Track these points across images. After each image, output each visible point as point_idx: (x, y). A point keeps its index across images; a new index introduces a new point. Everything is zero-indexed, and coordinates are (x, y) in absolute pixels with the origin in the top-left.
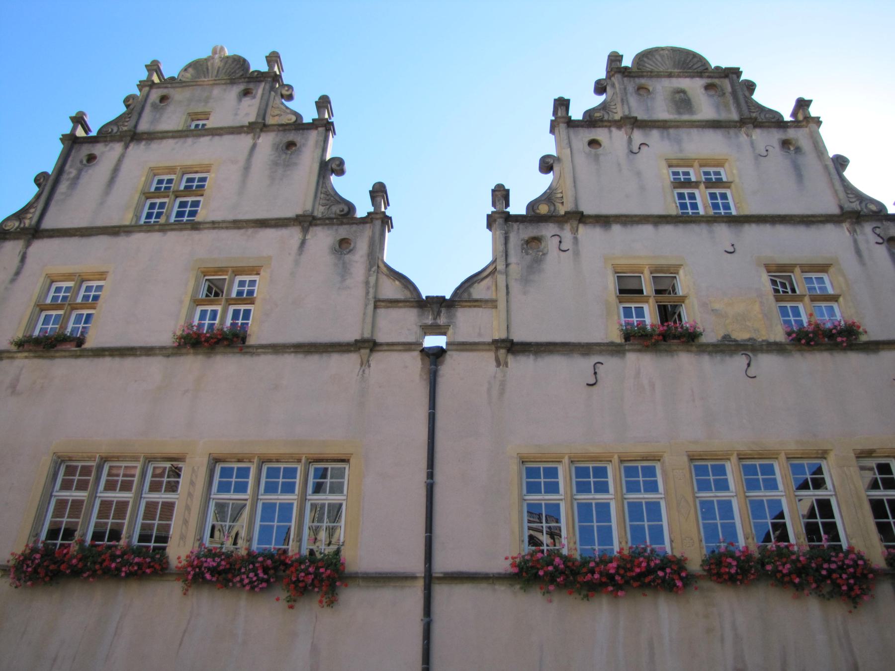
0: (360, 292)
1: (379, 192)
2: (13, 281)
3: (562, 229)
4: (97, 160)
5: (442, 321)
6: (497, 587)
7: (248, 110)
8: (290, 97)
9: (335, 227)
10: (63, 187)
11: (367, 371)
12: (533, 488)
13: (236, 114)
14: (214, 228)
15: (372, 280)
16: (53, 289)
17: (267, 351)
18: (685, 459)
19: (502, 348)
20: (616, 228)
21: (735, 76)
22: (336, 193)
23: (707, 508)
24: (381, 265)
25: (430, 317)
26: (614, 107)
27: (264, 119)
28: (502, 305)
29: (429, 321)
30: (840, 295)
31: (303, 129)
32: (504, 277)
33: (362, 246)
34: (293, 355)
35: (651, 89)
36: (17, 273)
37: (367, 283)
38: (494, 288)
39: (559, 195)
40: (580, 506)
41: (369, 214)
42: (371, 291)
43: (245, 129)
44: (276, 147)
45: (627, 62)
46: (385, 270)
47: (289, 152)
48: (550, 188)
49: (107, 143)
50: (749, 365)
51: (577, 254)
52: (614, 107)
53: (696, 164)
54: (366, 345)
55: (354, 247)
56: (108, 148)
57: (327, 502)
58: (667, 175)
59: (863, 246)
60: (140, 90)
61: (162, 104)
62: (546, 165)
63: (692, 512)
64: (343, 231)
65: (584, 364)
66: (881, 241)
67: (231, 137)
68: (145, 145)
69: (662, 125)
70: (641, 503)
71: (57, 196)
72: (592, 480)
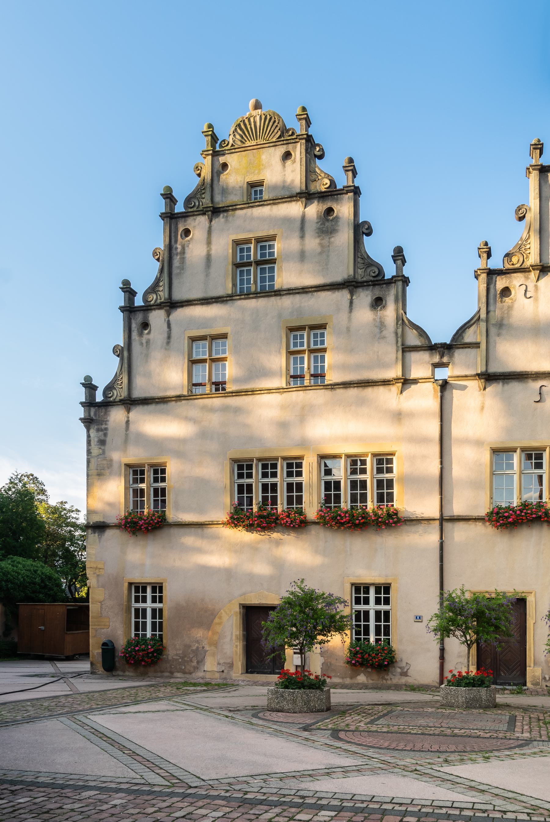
5: (445, 360)
6: (477, 523)
12: (240, 476)
15: (400, 331)
17: (340, 387)
22: (368, 256)
25: (438, 357)
28: (483, 346)
36: (169, 337)
37: (396, 334)
54: (399, 381)
64: (378, 292)
70: (293, 483)
71: (175, 271)
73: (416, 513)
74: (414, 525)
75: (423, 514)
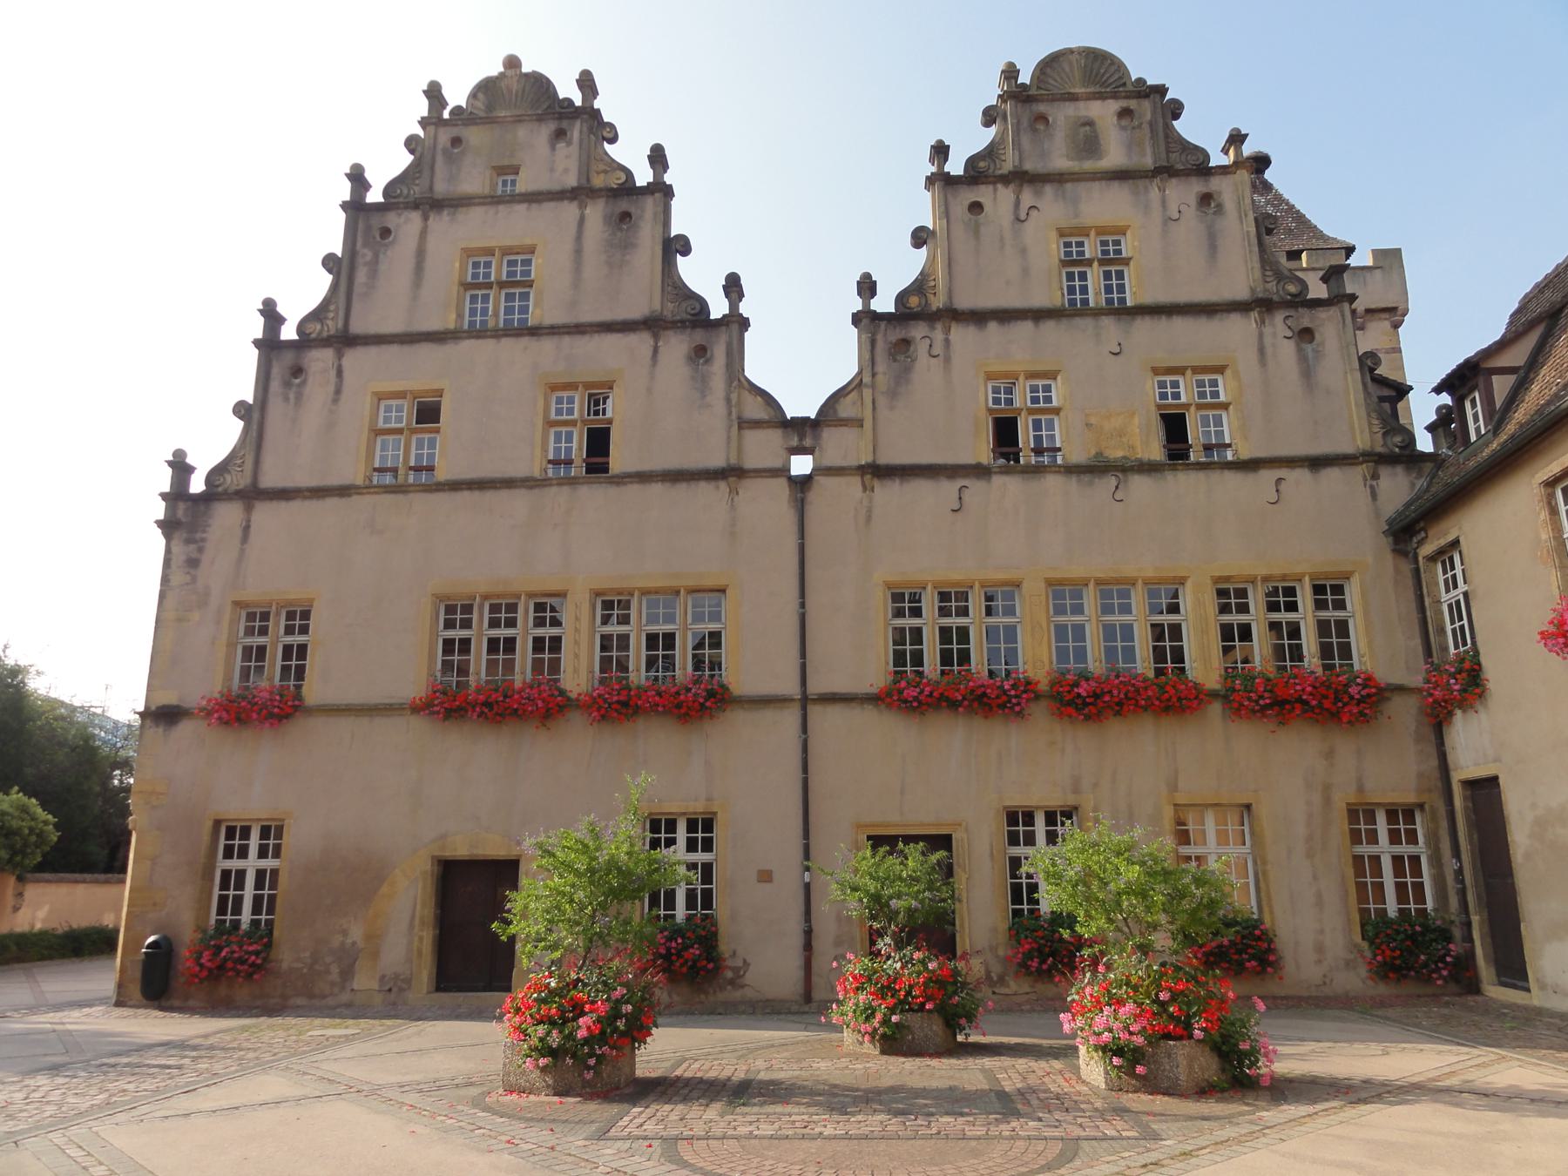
0: (719, 407)
1: (658, 158)
2: (335, 401)
3: (933, 328)
4: (393, 234)
5: (808, 442)
7: (564, 167)
8: (613, 140)
9: (689, 331)
10: (361, 276)
11: (736, 499)
13: (552, 170)
14: (554, 334)
16: (382, 408)
18: (1043, 585)
19: (868, 473)
20: (993, 326)
21: (1158, 97)
23: (1061, 631)
24: (742, 379)
27: (588, 180)
29: (795, 442)
30: (1230, 404)
31: (637, 194)
32: (871, 391)
33: (719, 353)
34: (660, 484)
35: (1050, 119)
36: (338, 391)
38: (859, 403)
39: (932, 283)
40: (942, 629)
41: (724, 316)
43: (568, 195)
44: (607, 219)
45: (1025, 78)
46: (745, 383)
47: (625, 227)
48: (921, 273)
49: (400, 211)
50: (1117, 488)
51: (947, 360)
53: (1093, 233)
55: (712, 355)
56: (402, 219)
58: (1055, 249)
59: (1268, 340)
60: (424, 128)
61: (456, 151)
62: (920, 237)
63: (1045, 638)
65: (948, 489)
66: (1289, 334)
67: (552, 204)
68: (448, 214)
69: (1059, 178)
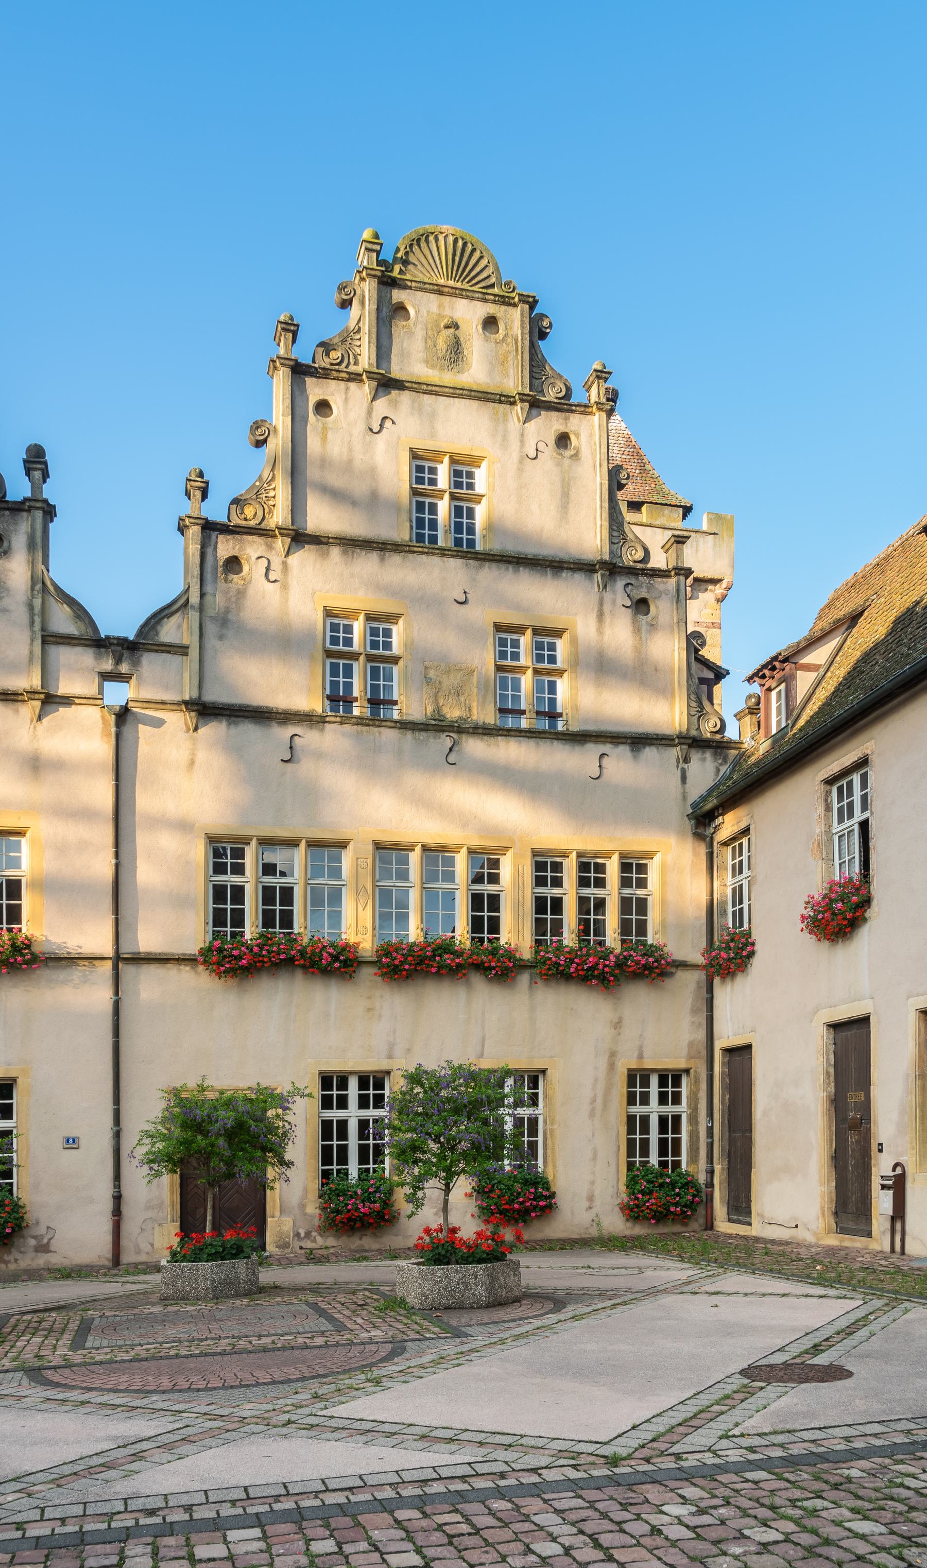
5: (124, 668)
6: (182, 967)
26: (358, 343)
28: (194, 652)
42: (38, 620)
52: (358, 343)
54: (37, 696)
55: (9, 547)
57: (229, 884)
72: (549, 874)
73: (68, 945)
74: (65, 967)
75: (81, 947)
